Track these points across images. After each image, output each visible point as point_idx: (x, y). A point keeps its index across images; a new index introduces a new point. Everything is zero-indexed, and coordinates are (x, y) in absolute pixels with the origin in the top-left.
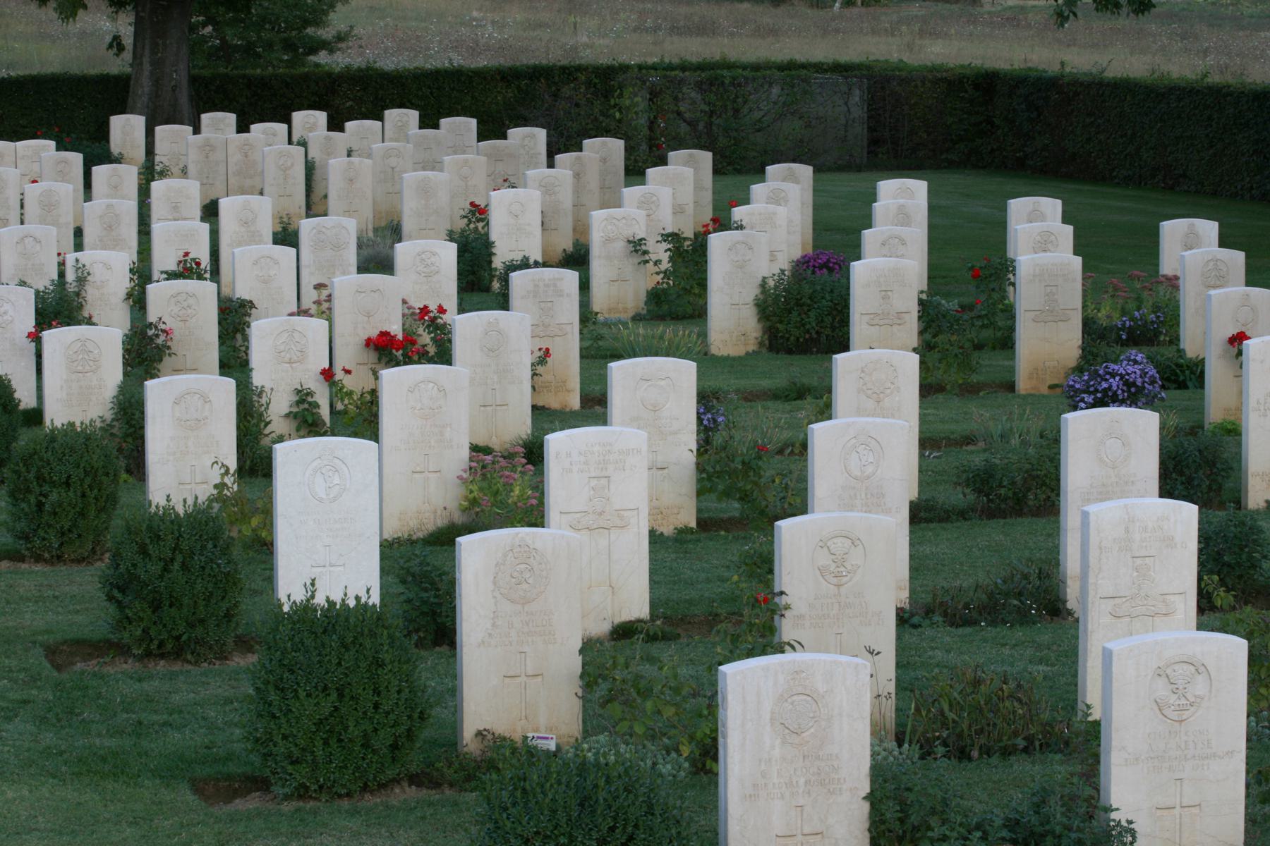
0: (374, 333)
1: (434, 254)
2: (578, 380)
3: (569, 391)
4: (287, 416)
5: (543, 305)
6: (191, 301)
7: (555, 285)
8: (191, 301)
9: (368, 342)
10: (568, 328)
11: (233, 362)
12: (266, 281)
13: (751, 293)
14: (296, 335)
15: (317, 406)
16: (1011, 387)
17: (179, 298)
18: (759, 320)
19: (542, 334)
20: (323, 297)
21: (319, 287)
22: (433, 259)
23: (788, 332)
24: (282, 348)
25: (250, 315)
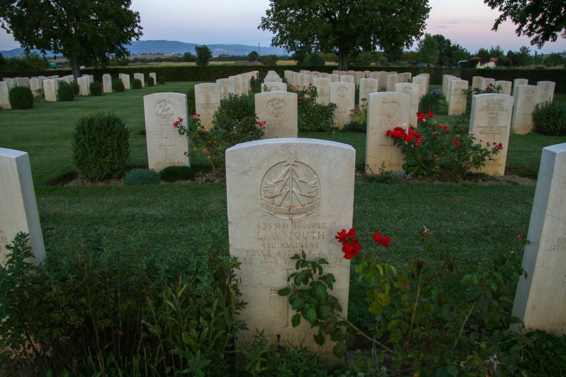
0: (392, 128)
1: (411, 88)
2: (505, 159)
3: (499, 165)
4: (282, 292)
5: (491, 115)
6: (281, 104)
7: (500, 104)
8: (281, 104)
9: (388, 133)
10: (504, 129)
11: (326, 129)
12: (342, 96)
13: (531, 110)
14: (300, 170)
15: (329, 279)
16: (446, 113)
17: (274, 102)
18: (533, 121)
19: (489, 132)
20: (365, 104)
21: (363, 99)
22: (410, 90)
23: (547, 126)
24: (277, 190)
25: (334, 110)
